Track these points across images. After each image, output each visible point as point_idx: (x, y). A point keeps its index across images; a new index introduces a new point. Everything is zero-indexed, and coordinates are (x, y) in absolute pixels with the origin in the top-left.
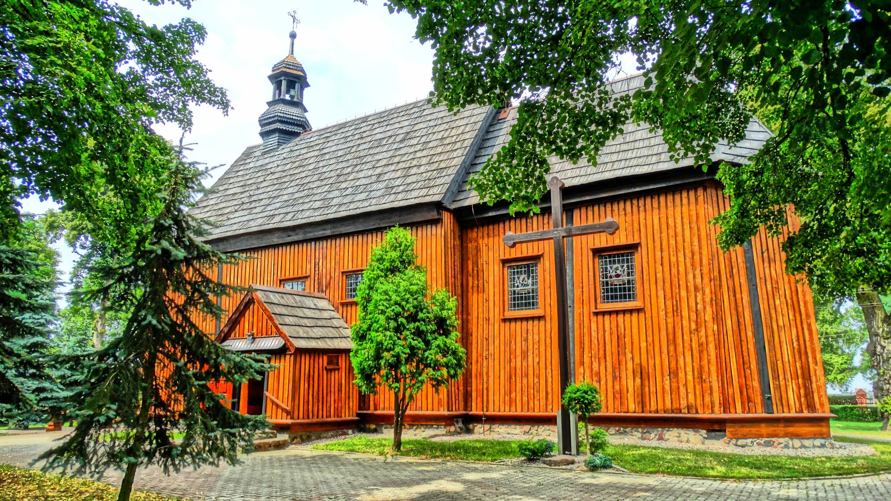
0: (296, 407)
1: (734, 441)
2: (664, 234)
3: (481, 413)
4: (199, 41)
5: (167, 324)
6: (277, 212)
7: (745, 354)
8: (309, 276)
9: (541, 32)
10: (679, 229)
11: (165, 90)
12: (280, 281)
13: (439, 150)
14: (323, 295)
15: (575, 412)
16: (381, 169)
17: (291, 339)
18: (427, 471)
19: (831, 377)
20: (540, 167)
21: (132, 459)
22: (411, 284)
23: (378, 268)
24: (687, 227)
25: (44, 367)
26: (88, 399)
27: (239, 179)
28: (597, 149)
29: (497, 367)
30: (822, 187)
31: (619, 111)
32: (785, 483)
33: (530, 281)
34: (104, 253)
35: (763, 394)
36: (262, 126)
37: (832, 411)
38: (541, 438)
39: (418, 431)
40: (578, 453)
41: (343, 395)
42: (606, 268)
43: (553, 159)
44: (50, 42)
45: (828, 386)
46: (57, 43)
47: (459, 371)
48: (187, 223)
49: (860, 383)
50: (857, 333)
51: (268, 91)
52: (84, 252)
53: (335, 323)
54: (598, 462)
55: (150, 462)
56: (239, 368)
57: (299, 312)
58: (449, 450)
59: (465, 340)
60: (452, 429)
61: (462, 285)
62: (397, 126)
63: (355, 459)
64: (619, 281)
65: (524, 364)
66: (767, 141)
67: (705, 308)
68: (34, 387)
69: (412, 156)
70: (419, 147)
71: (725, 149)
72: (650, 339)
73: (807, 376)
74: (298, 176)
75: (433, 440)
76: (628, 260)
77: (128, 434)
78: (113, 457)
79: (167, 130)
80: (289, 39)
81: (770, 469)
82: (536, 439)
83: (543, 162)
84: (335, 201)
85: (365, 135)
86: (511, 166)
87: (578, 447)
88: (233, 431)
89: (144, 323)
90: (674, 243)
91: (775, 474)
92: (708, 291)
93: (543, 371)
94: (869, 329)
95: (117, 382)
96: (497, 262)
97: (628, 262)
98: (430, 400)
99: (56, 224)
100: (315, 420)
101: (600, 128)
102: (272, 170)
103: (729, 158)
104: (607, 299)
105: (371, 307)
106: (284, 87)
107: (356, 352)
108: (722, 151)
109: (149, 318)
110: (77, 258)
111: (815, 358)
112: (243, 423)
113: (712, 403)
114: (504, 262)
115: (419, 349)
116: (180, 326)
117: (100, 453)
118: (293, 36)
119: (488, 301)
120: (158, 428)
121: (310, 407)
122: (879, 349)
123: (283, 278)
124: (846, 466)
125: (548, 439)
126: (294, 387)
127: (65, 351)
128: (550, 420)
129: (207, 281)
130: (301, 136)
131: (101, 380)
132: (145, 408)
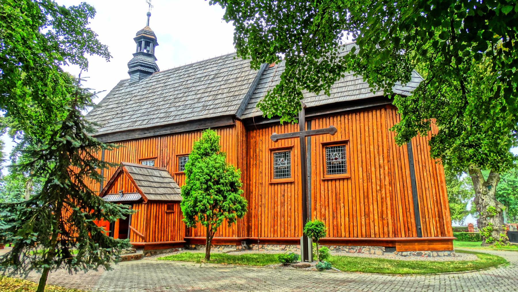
1: (400, 253)
3: (257, 238)
5: (68, 185)
6: (138, 119)
7: (407, 203)
10: (371, 133)
12: (140, 160)
13: (235, 84)
16: (200, 95)
17: (145, 195)
19: (454, 217)
22: (216, 163)
23: (197, 153)
26: (20, 230)
29: (266, 212)
31: (342, 64)
32: (428, 276)
33: (286, 162)
35: (416, 226)
36: (130, 68)
37: (455, 236)
40: (312, 261)
42: (330, 155)
43: (306, 93)
46: (5, 13)
48: (82, 124)
49: (471, 220)
50: (469, 191)
51: (133, 47)
52: (19, 141)
53: (172, 185)
54: (323, 266)
55: (58, 267)
56: (113, 212)
57: (151, 179)
58: (238, 260)
59: (248, 195)
60: (240, 247)
61: (247, 163)
62: (210, 70)
64: (337, 162)
65: (282, 210)
67: (385, 177)
69: (218, 88)
70: (223, 83)
72: (354, 196)
73: (441, 216)
74: (151, 98)
75: (229, 254)
76: (342, 150)
78: (35, 265)
79: (71, 69)
80: (147, 17)
85: (191, 75)
86: (281, 96)
92: (386, 168)
96: (267, 150)
97: (342, 151)
98: (227, 231)
100: (159, 242)
102: (135, 94)
104: (330, 172)
105: (192, 177)
108: (398, 88)
110: (15, 145)
111: (445, 206)
114: (271, 150)
115: (220, 201)
117: (27, 261)
118: (149, 15)
120: (63, 247)
121: (157, 235)
122: (480, 201)
123: (141, 158)
124: (462, 267)
128: (296, 242)
129: (95, 160)
130: (153, 75)
132: (55, 235)
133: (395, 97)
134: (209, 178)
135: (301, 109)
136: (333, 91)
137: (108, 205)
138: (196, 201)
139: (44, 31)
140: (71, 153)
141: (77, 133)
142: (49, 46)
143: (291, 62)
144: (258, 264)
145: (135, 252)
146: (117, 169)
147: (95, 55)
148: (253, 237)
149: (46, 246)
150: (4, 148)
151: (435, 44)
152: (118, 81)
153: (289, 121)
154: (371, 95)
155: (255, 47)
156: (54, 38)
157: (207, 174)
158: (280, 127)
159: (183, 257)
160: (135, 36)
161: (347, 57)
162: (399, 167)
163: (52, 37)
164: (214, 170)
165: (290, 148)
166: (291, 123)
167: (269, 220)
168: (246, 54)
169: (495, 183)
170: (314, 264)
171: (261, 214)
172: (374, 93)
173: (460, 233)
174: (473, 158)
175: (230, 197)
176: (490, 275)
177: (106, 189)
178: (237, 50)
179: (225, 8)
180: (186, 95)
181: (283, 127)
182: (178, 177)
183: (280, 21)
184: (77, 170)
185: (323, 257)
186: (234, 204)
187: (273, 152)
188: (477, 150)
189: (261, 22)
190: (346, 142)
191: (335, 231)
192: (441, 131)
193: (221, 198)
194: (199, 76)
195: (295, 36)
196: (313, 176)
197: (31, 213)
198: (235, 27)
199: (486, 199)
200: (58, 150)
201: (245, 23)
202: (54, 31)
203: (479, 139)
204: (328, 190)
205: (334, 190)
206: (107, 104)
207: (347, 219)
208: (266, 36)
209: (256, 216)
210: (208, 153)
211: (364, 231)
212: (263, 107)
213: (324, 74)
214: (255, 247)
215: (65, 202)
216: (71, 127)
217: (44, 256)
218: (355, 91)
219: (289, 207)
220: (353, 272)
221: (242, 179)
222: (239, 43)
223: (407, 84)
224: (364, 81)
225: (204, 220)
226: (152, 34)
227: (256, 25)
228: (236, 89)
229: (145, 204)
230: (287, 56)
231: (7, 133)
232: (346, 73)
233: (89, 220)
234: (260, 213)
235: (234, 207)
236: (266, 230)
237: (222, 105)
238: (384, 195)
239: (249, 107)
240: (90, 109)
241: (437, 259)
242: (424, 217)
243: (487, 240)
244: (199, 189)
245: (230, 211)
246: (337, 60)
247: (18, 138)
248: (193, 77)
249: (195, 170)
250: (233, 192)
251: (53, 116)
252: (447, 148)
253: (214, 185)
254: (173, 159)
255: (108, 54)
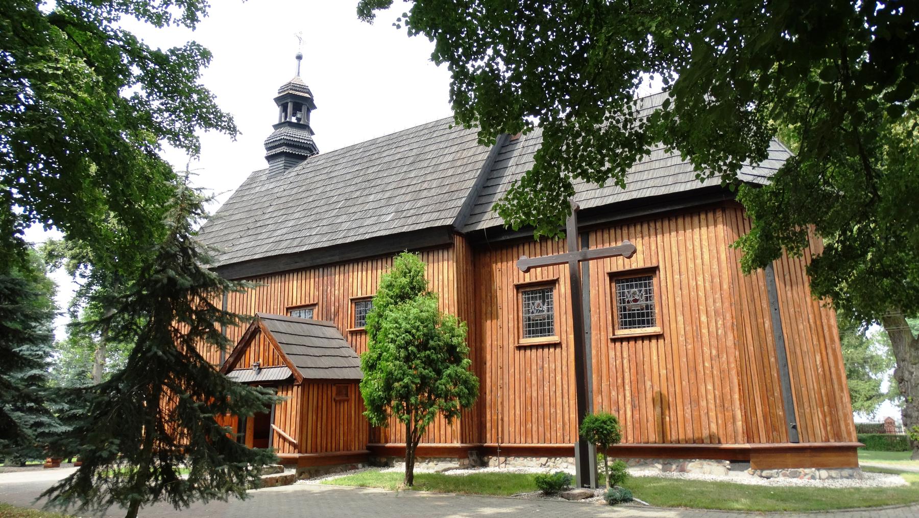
3: (496, 445)
6: (284, 238)
12: (287, 309)
13: (450, 172)
16: (391, 192)
23: (388, 295)
29: (512, 397)
33: (545, 307)
36: (268, 149)
37: (860, 440)
40: (597, 487)
43: (579, 184)
46: (58, 69)
48: (193, 250)
51: (274, 114)
52: (84, 281)
53: (344, 352)
54: (618, 495)
55: (156, 499)
61: (475, 311)
65: (540, 393)
69: (422, 179)
74: (305, 201)
86: (535, 191)
96: (511, 287)
102: (278, 195)
105: (380, 336)
108: (747, 172)
110: (78, 288)
114: (518, 287)
120: (163, 463)
121: (319, 440)
123: (290, 305)
124: (876, 498)
128: (566, 452)
129: (213, 309)
130: (308, 160)
133: (742, 188)
135: (570, 214)
137: (239, 389)
139: (126, 93)
142: (136, 119)
143: (553, 133)
144: (499, 491)
146: (248, 326)
147: (212, 130)
148: (488, 444)
149: (134, 462)
150: (58, 294)
152: (248, 174)
153: (551, 235)
154: (698, 185)
155: (488, 109)
156: (143, 105)
157: (407, 331)
158: (532, 246)
160: (277, 95)
161: (656, 115)
162: (752, 313)
163: (140, 102)
164: (418, 323)
165: (553, 283)
166: (552, 238)
167: (518, 412)
168: (471, 119)
170: (600, 491)
171: (502, 403)
172: (702, 180)
173: (870, 435)
174: (890, 297)
175: (448, 372)
177: (231, 360)
178: (456, 113)
179: (435, 41)
180: (365, 193)
181: (538, 246)
182: (354, 337)
183: (530, 60)
184: (185, 329)
185: (616, 478)
186: (455, 385)
187: (521, 290)
188: (899, 282)
189: (497, 64)
192: (829, 248)
193: (433, 374)
194: (387, 159)
195: (555, 83)
196: (594, 333)
197: (109, 403)
198: (451, 73)
200: (152, 295)
201: (469, 66)
202: (143, 94)
203: (901, 261)
206: (231, 212)
208: (507, 87)
210: (407, 293)
212: (503, 211)
213: (612, 150)
214: (493, 461)
215: (165, 384)
217: (132, 478)
218: (667, 178)
220: (673, 506)
221: (468, 339)
222: (458, 99)
223: (761, 164)
224: (683, 160)
226: (305, 89)
227: (487, 69)
229: (298, 386)
230: (543, 120)
231: (63, 267)
233: (206, 415)
234: (500, 400)
236: (512, 430)
237: (430, 208)
239: (477, 212)
240: (203, 222)
246: (637, 123)
247: (83, 276)
248: (378, 162)
250: (452, 363)
251: (146, 236)
253: (419, 351)
255: (234, 128)
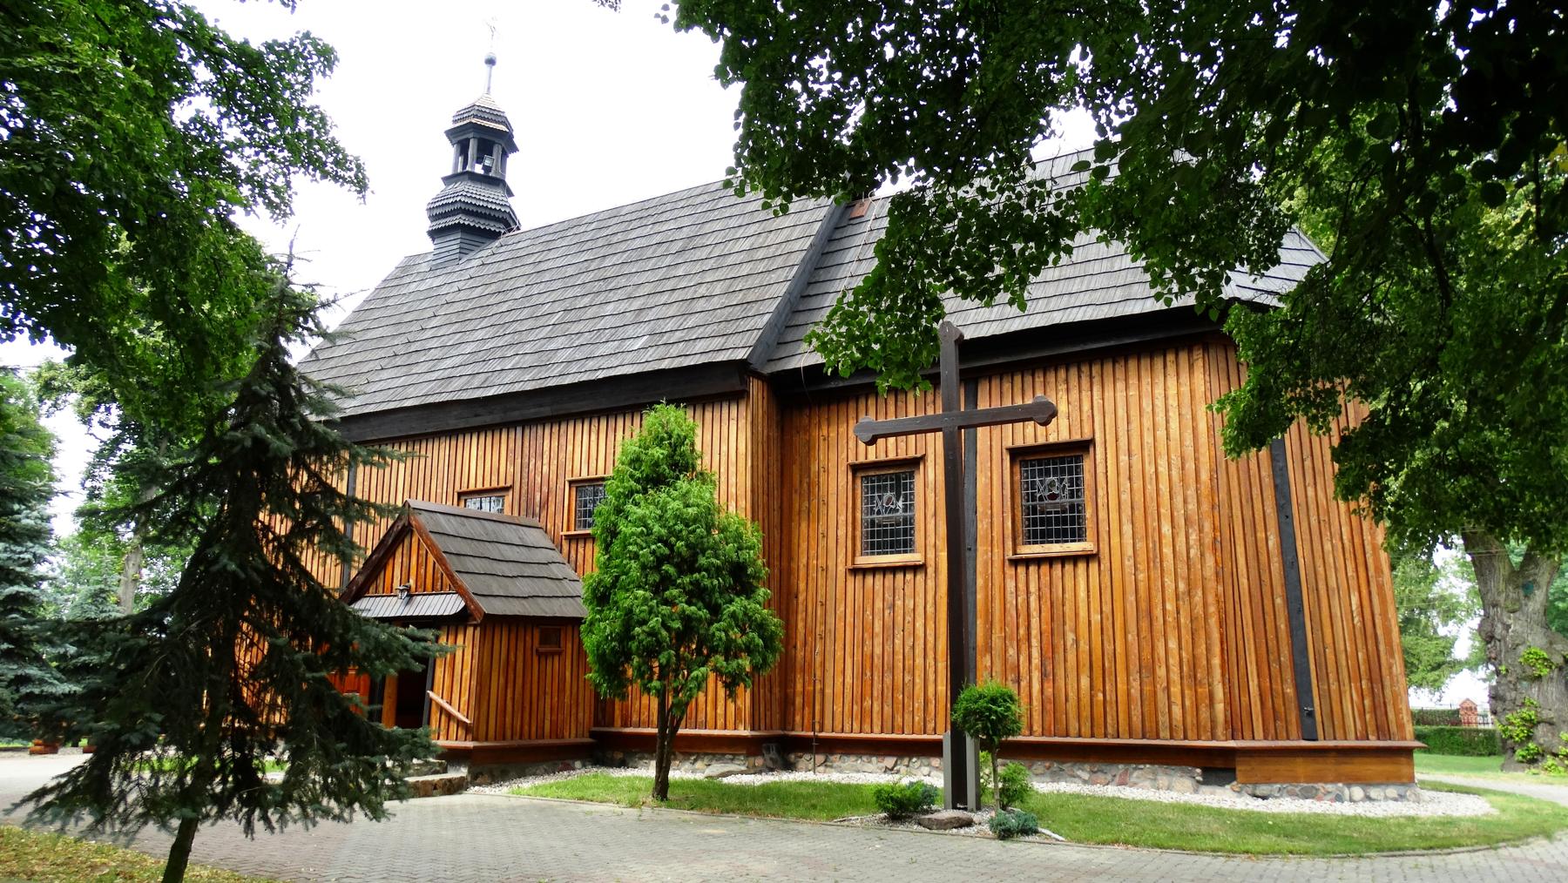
0: (483, 719)
1: (1250, 788)
2: (1135, 425)
4: (324, 74)
5: (256, 569)
6: (456, 372)
7: (1271, 636)
8: (511, 487)
9: (926, 72)
11: (257, 154)
12: (460, 495)
13: (745, 269)
14: (535, 521)
15: (975, 735)
16: (642, 300)
17: (476, 598)
18: (714, 836)
19: (1415, 678)
20: (926, 312)
21: (188, 812)
22: (687, 506)
23: (632, 476)
24: (1173, 415)
25: (31, 642)
26: (113, 702)
27: (389, 312)
28: (1023, 282)
29: (839, 654)
30: (1402, 351)
31: (1065, 214)
32: (1335, 862)
33: (900, 504)
34: (141, 437)
35: (1300, 709)
36: (434, 218)
37: (1418, 737)
38: (914, 780)
39: (699, 765)
40: (979, 808)
41: (567, 700)
42: (1033, 483)
43: (951, 301)
44: (59, 64)
45: (1411, 691)
46: (72, 66)
47: (770, 658)
48: (298, 391)
49: (1467, 690)
50: (1463, 600)
51: (446, 158)
52: (108, 434)
53: (556, 571)
54: (1013, 822)
55: (221, 815)
56: (385, 651)
57: (493, 551)
58: (753, 799)
59: (785, 601)
60: (759, 761)
61: (781, 508)
62: (672, 225)
63: (586, 813)
64: (1055, 505)
65: (888, 648)
66: (1313, 269)
68: (11, 675)
69: (697, 279)
70: (710, 264)
71: (1247, 280)
72: (1107, 609)
73: (1376, 676)
74: (495, 309)
75: (725, 780)
77: (182, 766)
78: (155, 807)
79: (254, 223)
80: (486, 67)
81: (1311, 837)
82: (905, 781)
83: (934, 303)
84: (563, 356)
85: (615, 239)
86: (878, 311)
87: (978, 797)
88: (373, 760)
89: (215, 568)
90: (1151, 440)
91: (1320, 845)
92: (1207, 527)
93: (919, 661)
94: (1482, 594)
95: (165, 670)
96: (843, 468)
98: (720, 711)
99: (56, 384)
100: (516, 742)
101: (1032, 244)
102: (448, 298)
103: (1246, 295)
105: (616, 548)
106: (472, 151)
107: (592, 624)
108: (1240, 284)
109: (224, 560)
110: (96, 446)
111: (1389, 643)
112: (392, 746)
113: (1213, 721)
114: (856, 469)
115: (700, 620)
116: (281, 574)
117: (131, 798)
119: (826, 536)
120: (238, 755)
121: (508, 720)
122: (1499, 630)
123: (464, 489)
124: (1441, 834)
125: (927, 781)
126: (479, 683)
127: (67, 614)
128: (929, 749)
129: (331, 492)
130: (502, 240)
131: (136, 668)
132: (214, 718)
134: (667, 551)
136: (1033, 290)
137: (374, 631)
138: (629, 620)
140: (266, 472)
141: (282, 415)
145: (445, 771)
151: (1352, 149)
159: (587, 788)
160: (451, 126)
167: (848, 680)
169: (1547, 576)
176: (1532, 862)
179: (721, 42)
182: (573, 546)
184: (282, 526)
185: (1010, 794)
186: (743, 632)
187: (860, 475)
190: (1085, 446)
191: (1049, 718)
199: (1516, 625)
204: (1028, 592)
205: (1046, 590)
207: (1085, 682)
209: (808, 667)
211: (1136, 720)
216: (267, 399)
219: (909, 642)
221: (767, 553)
225: (650, 679)
226: (499, 117)
228: (750, 283)
232: (1081, 238)
235: (741, 640)
236: (838, 709)
238: (1199, 610)
241: (1364, 809)
242: (1323, 676)
243: (1520, 752)
244: (639, 587)
245: (731, 651)
249: (625, 528)
251: (210, 368)
252: (1390, 472)
254: (560, 493)
